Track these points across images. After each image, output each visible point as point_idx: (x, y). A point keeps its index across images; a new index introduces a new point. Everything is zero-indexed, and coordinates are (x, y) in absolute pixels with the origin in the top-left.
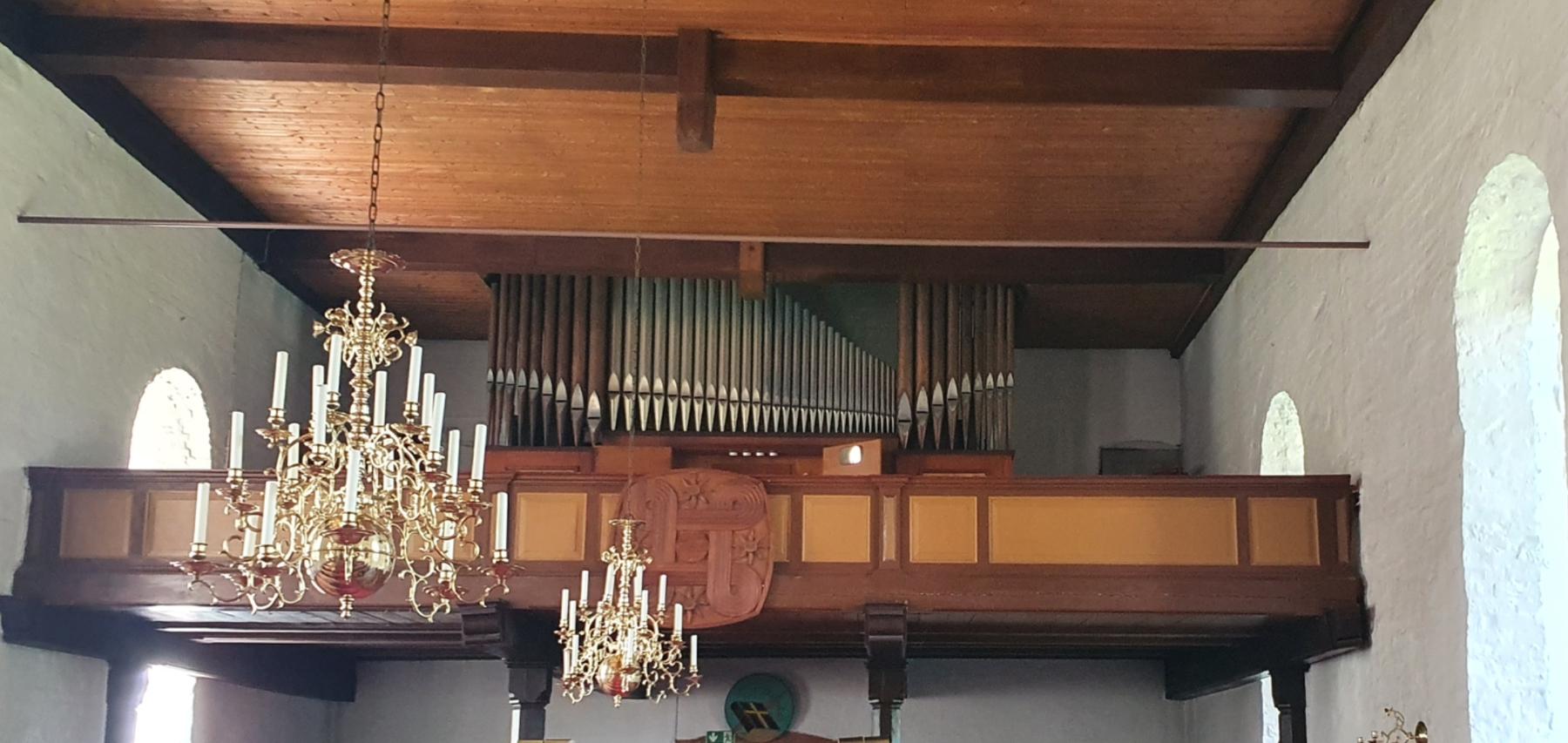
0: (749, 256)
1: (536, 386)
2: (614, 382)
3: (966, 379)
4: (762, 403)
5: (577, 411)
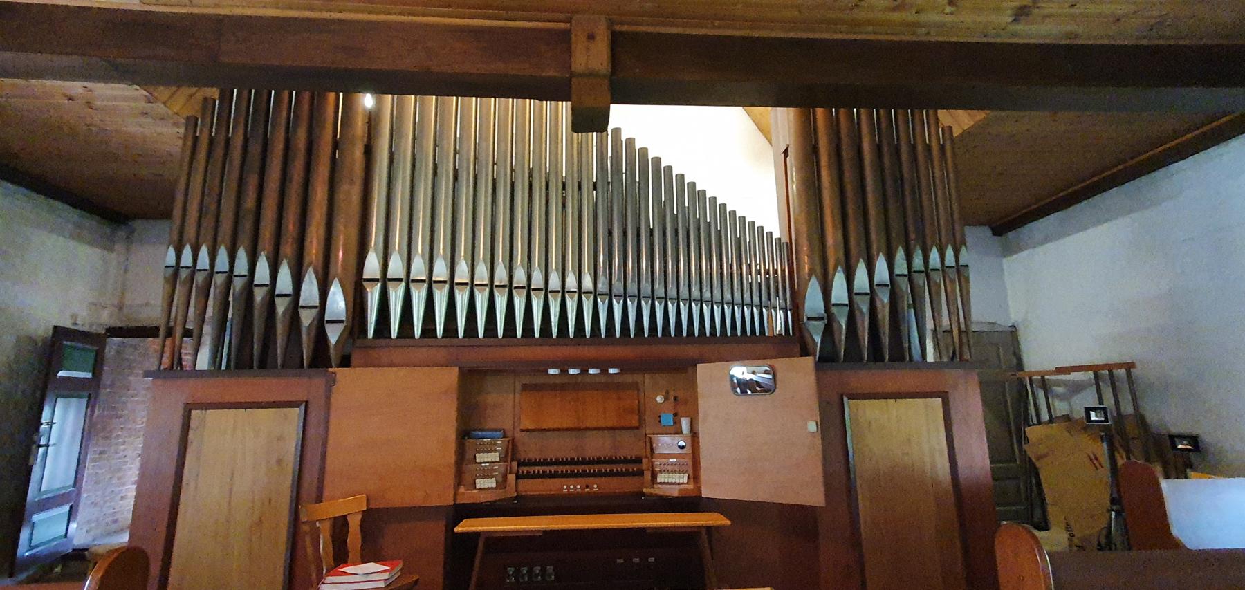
0: (588, 49)
1: (316, 301)
2: (372, 265)
3: (900, 255)
4: (595, 294)
5: (308, 311)
